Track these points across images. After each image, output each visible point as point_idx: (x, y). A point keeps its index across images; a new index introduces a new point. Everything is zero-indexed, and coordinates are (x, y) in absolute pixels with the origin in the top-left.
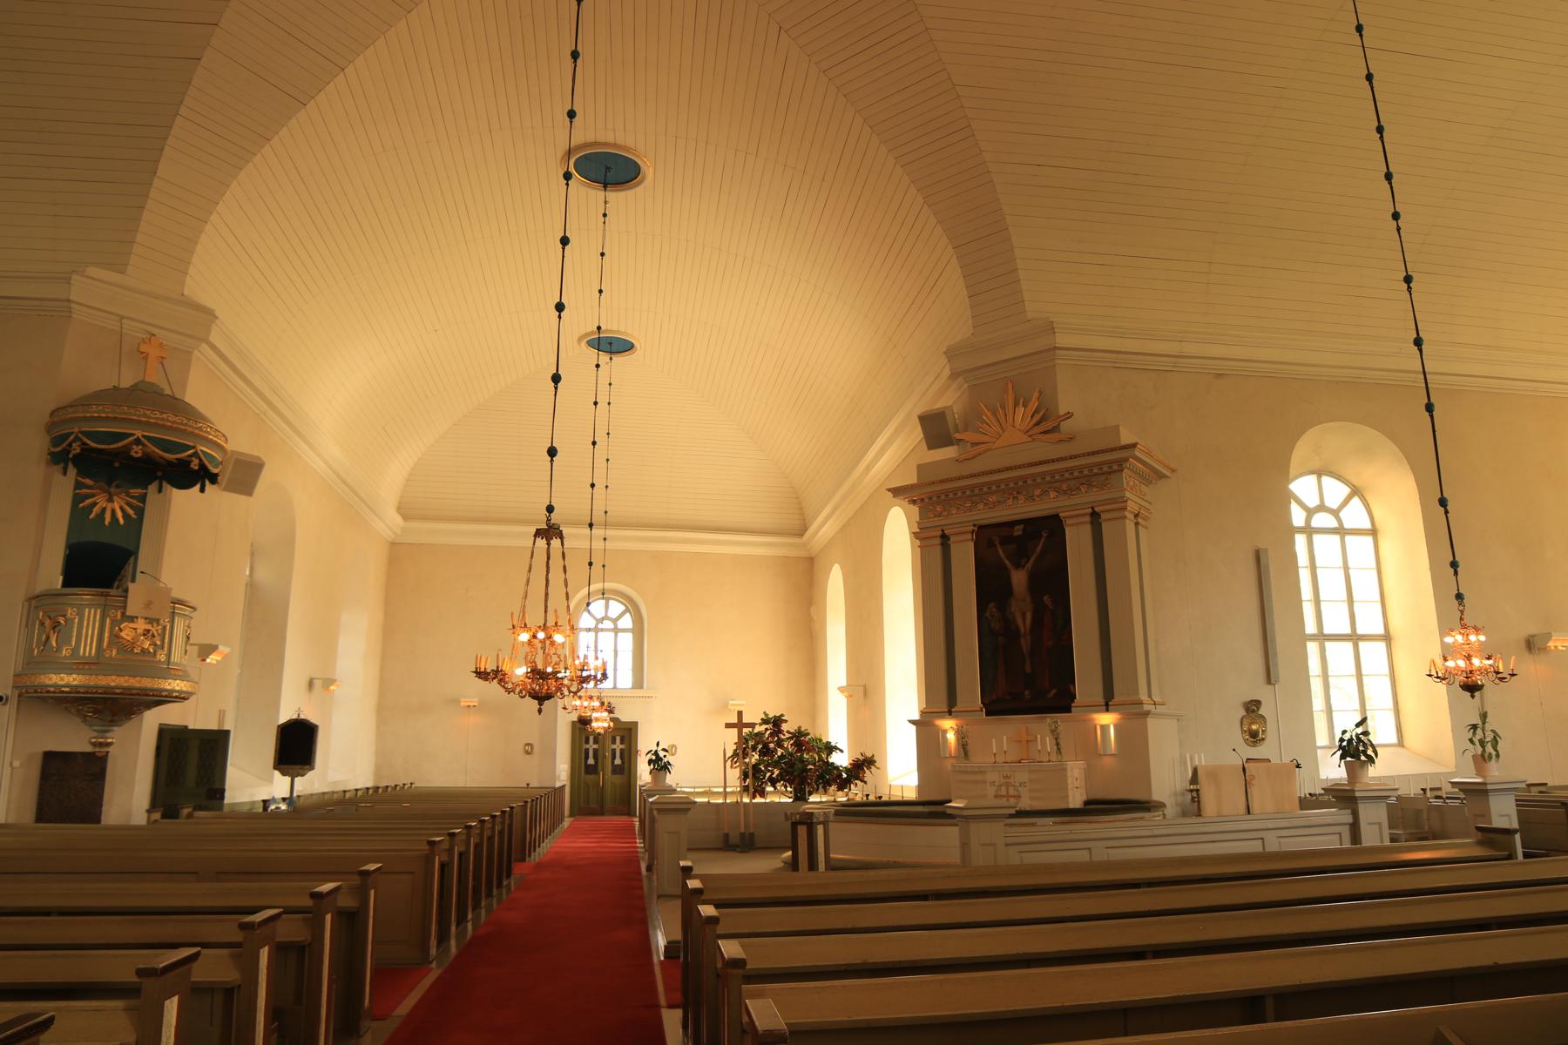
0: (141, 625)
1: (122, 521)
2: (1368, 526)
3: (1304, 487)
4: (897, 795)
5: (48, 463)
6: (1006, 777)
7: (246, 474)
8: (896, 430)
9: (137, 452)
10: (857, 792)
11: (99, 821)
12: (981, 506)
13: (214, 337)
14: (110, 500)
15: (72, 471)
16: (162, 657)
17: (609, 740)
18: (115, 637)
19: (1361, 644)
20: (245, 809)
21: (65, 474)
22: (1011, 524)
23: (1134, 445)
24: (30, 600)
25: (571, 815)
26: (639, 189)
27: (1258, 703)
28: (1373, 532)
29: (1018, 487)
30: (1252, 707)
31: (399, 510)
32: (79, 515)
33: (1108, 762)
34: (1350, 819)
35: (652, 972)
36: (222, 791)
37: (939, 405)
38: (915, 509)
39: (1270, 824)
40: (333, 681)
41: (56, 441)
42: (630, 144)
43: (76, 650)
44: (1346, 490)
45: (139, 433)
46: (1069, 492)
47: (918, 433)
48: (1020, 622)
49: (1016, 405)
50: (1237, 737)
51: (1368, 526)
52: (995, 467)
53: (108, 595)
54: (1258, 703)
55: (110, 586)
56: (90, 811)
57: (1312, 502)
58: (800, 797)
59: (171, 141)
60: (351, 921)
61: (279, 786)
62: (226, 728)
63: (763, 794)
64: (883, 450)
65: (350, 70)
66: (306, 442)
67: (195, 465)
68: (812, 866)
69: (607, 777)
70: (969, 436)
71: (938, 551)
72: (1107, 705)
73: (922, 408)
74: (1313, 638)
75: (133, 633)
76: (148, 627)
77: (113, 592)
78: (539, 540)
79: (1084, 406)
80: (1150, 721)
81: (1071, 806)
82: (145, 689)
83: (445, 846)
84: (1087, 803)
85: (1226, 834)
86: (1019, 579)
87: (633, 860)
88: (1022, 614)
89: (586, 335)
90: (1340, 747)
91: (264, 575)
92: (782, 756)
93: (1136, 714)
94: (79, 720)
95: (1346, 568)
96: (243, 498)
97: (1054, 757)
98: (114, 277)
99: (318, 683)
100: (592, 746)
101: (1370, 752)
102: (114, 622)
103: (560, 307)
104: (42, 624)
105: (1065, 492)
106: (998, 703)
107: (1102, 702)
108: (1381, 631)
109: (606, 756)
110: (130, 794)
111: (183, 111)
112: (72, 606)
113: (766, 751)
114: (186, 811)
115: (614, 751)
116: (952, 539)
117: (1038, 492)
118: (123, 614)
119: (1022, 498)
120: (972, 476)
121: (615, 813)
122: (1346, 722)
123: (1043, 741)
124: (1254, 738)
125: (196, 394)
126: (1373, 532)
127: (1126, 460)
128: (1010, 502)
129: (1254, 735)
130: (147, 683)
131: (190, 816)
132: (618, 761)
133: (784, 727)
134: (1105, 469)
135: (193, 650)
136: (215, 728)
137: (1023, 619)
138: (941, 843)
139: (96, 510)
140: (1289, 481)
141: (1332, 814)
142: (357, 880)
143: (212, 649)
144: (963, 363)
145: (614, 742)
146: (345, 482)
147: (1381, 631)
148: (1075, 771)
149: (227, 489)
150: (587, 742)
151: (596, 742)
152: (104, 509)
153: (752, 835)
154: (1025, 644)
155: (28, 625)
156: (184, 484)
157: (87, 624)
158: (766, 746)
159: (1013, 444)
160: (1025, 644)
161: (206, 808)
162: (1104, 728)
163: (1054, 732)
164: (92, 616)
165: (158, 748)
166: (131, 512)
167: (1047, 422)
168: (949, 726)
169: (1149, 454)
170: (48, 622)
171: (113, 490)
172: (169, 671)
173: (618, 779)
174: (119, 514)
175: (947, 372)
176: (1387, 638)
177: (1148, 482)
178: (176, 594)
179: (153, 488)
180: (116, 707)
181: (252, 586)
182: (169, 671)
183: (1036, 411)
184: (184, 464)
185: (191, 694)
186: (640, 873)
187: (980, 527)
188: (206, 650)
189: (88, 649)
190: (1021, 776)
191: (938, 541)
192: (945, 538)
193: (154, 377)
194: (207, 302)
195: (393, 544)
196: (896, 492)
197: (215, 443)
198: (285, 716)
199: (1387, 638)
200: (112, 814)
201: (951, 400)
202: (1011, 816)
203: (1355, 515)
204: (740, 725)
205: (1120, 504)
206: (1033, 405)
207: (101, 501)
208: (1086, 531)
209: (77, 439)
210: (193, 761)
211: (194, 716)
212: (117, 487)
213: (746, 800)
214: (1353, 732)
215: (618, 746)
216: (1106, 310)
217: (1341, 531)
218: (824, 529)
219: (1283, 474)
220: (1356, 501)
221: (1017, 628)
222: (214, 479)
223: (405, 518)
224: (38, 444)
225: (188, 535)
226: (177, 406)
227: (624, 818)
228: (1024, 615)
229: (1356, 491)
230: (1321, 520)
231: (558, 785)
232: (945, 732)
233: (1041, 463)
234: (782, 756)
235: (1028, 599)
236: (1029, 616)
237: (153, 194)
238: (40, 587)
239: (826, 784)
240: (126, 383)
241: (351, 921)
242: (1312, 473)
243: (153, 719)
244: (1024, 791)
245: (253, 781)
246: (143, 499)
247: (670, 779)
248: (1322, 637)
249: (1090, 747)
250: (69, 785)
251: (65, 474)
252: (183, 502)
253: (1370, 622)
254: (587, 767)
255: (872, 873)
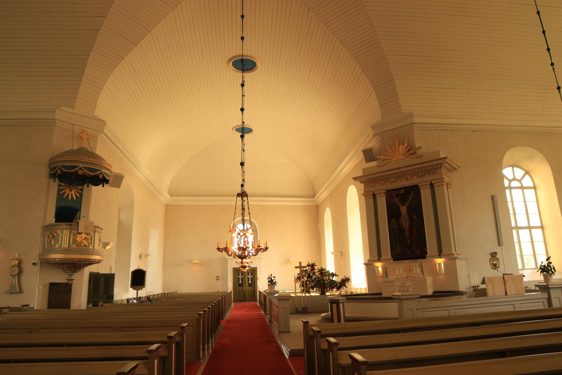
0: (84, 236)
1: (75, 198)
2: (532, 185)
3: (507, 172)
4: (359, 292)
5: (49, 178)
6: (403, 284)
7: (118, 180)
8: (351, 157)
9: (80, 172)
10: (343, 291)
11: (69, 308)
12: (388, 183)
13: (105, 131)
14: (71, 191)
15: (57, 181)
16: (91, 247)
17: (246, 274)
18: (75, 240)
19: (532, 230)
20: (119, 302)
21: (55, 181)
22: (400, 189)
23: (446, 158)
24: (43, 227)
25: (234, 302)
26: (255, 72)
27: (496, 253)
28: (535, 188)
29: (401, 176)
30: (494, 255)
31: (168, 193)
32: (60, 196)
33: (441, 277)
34: (547, 296)
35: (287, 362)
36: (113, 296)
37: (369, 146)
38: (362, 185)
39: (517, 299)
40: (148, 255)
41: (52, 170)
42: (252, 55)
43: (61, 245)
44: (523, 172)
45: (81, 166)
46: (421, 176)
47: (362, 156)
48: (404, 224)
49: (399, 145)
50: (488, 266)
51: (532, 185)
52: (392, 168)
53: (72, 225)
54: (496, 253)
55: (71, 222)
56: (66, 305)
57: (511, 177)
58: (323, 293)
59: (89, 60)
60: (179, 345)
61: (132, 294)
62: (113, 273)
63: (309, 292)
64: (346, 164)
65: (153, 31)
66: (137, 168)
67: (101, 177)
68: (339, 321)
69: (246, 288)
70: (382, 157)
71: (372, 200)
72: (440, 255)
73: (363, 147)
74: (514, 228)
75: (81, 239)
76: (86, 236)
77: (73, 224)
78: (238, 198)
79: (425, 144)
80: (457, 261)
81: (429, 294)
82: (86, 259)
83: (203, 315)
84: (434, 293)
85: (497, 304)
86: (403, 209)
87: (262, 319)
88: (405, 223)
89: (235, 127)
90: (541, 268)
91: (123, 217)
92: (315, 278)
93: (451, 259)
94: (62, 271)
95: (525, 202)
96: (116, 189)
97: (421, 276)
98: (70, 110)
99: (143, 256)
100: (240, 277)
101: (553, 270)
102: (74, 235)
103: (242, 110)
104: (49, 236)
105: (420, 176)
106: (398, 256)
107: (438, 254)
108: (540, 225)
109: (245, 279)
110: (80, 298)
111: (94, 49)
112: (59, 229)
113: (309, 277)
114: (101, 304)
115: (248, 278)
116: (377, 195)
117: (409, 177)
118: (77, 232)
119: (403, 179)
120: (406, 167)
121: (250, 300)
122: (542, 260)
123: (416, 270)
124: (495, 266)
125: (100, 151)
126: (535, 188)
127: (443, 163)
128: (399, 181)
129: (495, 265)
130: (86, 257)
131: (102, 305)
132: (250, 282)
133: (315, 267)
134: (435, 167)
135: (101, 245)
136: (108, 273)
137: (406, 224)
138: (390, 310)
139: (66, 194)
140: (502, 169)
141: (540, 294)
142: (180, 330)
143: (108, 244)
144: (378, 130)
145: (248, 275)
146: (151, 183)
147: (540, 225)
148: (429, 280)
149: (112, 186)
150: (239, 275)
151: (242, 275)
152: (68, 194)
153: (306, 308)
154: (407, 234)
155: (43, 236)
156: (96, 184)
157: (64, 235)
158: (309, 274)
159: (398, 159)
160: (407, 234)
161: (107, 302)
162: (440, 264)
163: (421, 266)
164: (66, 233)
165: (90, 281)
166: (78, 195)
167: (411, 151)
168: (379, 266)
169: (451, 161)
170: (50, 236)
171: (71, 187)
172: (94, 252)
173: (250, 288)
174: (74, 196)
175: (372, 134)
176: (542, 227)
177: (450, 172)
178: (96, 224)
179: (85, 186)
180: (75, 266)
181: (119, 221)
182: (94, 252)
183: (407, 147)
184: (97, 177)
185: (102, 260)
186: (266, 323)
187: (388, 191)
188: (106, 244)
189: (65, 245)
190: (409, 283)
191: (372, 196)
192: (374, 195)
193: (86, 145)
194: (103, 119)
195: (167, 205)
196: (355, 179)
197: (108, 169)
198: (133, 268)
199: (542, 227)
200: (74, 305)
201: (373, 144)
202: (418, 298)
203: (527, 182)
204: (300, 267)
205: (441, 180)
206: (406, 144)
207: (67, 191)
208: (429, 190)
209: (59, 168)
210: (102, 285)
211: (102, 269)
212: (73, 186)
213: (304, 295)
214: (545, 263)
215: (250, 276)
216: (432, 107)
217: (522, 188)
218: (322, 195)
219: (500, 166)
220: (527, 176)
221: (404, 228)
222: (107, 182)
223: (171, 196)
224: (45, 171)
225: (99, 202)
226: (94, 156)
227: (254, 303)
228: (406, 223)
229: (527, 173)
230: (515, 184)
231: (229, 291)
232: (378, 267)
233: (410, 166)
234: (315, 278)
235: (407, 217)
236: (408, 223)
237: (83, 79)
238: (47, 223)
239: (333, 288)
240: (76, 148)
241: (179, 345)
242: (510, 166)
243: (88, 270)
244: (410, 289)
245: (124, 292)
246: (82, 190)
247: (277, 288)
248: (518, 228)
249: (434, 272)
250: (59, 295)
251: (55, 181)
252: (96, 191)
253: (535, 222)
254: (239, 284)
255: (376, 322)
